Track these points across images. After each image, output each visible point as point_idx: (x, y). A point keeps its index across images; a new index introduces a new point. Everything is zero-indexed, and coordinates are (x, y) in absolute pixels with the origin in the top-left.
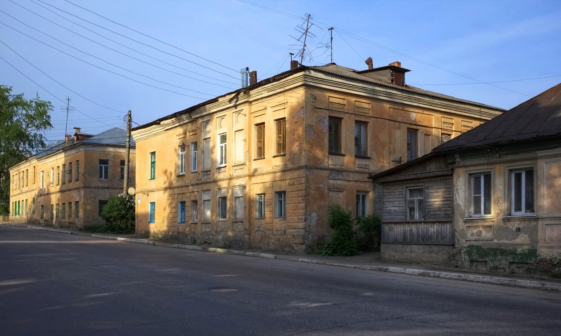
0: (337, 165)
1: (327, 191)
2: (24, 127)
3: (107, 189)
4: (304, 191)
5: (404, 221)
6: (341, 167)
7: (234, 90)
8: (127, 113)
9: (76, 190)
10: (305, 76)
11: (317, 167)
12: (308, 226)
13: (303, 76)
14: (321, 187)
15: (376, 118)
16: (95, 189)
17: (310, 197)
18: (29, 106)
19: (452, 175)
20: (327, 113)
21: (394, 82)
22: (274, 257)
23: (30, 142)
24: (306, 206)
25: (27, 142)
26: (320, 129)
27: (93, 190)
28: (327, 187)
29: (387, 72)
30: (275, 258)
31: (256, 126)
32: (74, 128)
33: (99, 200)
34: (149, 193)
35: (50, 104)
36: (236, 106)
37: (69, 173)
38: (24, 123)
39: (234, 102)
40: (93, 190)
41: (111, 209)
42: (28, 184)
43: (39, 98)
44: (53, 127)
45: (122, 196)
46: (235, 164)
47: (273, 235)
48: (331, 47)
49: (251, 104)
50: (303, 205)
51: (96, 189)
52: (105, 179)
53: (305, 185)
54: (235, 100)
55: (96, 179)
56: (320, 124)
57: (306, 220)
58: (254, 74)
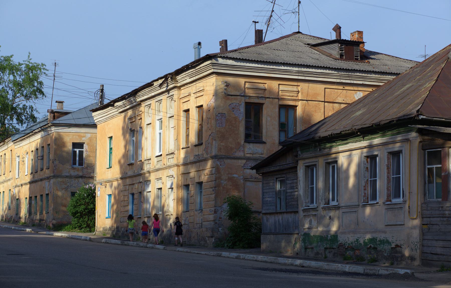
0: (255, 154)
1: (242, 181)
2: (10, 97)
3: (81, 179)
4: (214, 182)
5: (274, 211)
6: (260, 155)
7: (162, 75)
8: (99, 87)
9: (47, 180)
10: (212, 64)
11: (228, 157)
12: (218, 218)
13: (211, 64)
14: (234, 177)
15: (306, 100)
16: (67, 179)
17: (221, 188)
18: (18, 70)
19: (296, 167)
20: (243, 100)
21: (344, 56)
22: (163, 248)
23: (19, 116)
24: (216, 197)
25: (15, 117)
26: (234, 116)
27: (64, 179)
28: (242, 177)
29: (336, 46)
30: (164, 249)
31: (185, 113)
32: (56, 102)
33: (72, 192)
34: (107, 183)
35: (44, 67)
36: (168, 91)
37: (41, 159)
38: (10, 92)
39: (165, 87)
40: (65, 180)
41: (78, 203)
42: (6, 173)
43: (30, 59)
44: (45, 96)
45: (91, 187)
46: (168, 152)
47: (194, 228)
48: (299, 12)
49: (180, 89)
50: (214, 195)
51: (68, 179)
52: (80, 167)
53: (215, 176)
54: (165, 85)
55: (68, 166)
56: (233, 111)
57: (215, 212)
58: (224, 43)
